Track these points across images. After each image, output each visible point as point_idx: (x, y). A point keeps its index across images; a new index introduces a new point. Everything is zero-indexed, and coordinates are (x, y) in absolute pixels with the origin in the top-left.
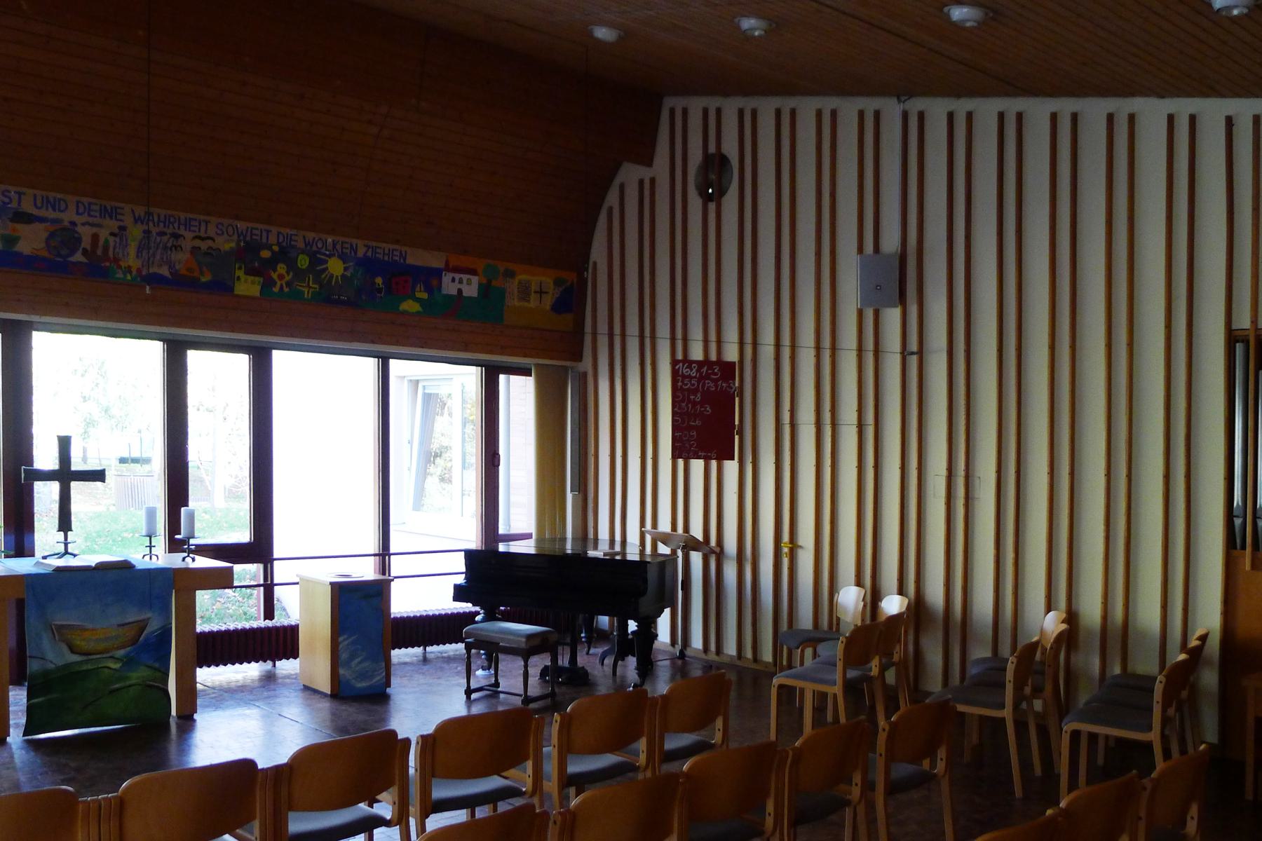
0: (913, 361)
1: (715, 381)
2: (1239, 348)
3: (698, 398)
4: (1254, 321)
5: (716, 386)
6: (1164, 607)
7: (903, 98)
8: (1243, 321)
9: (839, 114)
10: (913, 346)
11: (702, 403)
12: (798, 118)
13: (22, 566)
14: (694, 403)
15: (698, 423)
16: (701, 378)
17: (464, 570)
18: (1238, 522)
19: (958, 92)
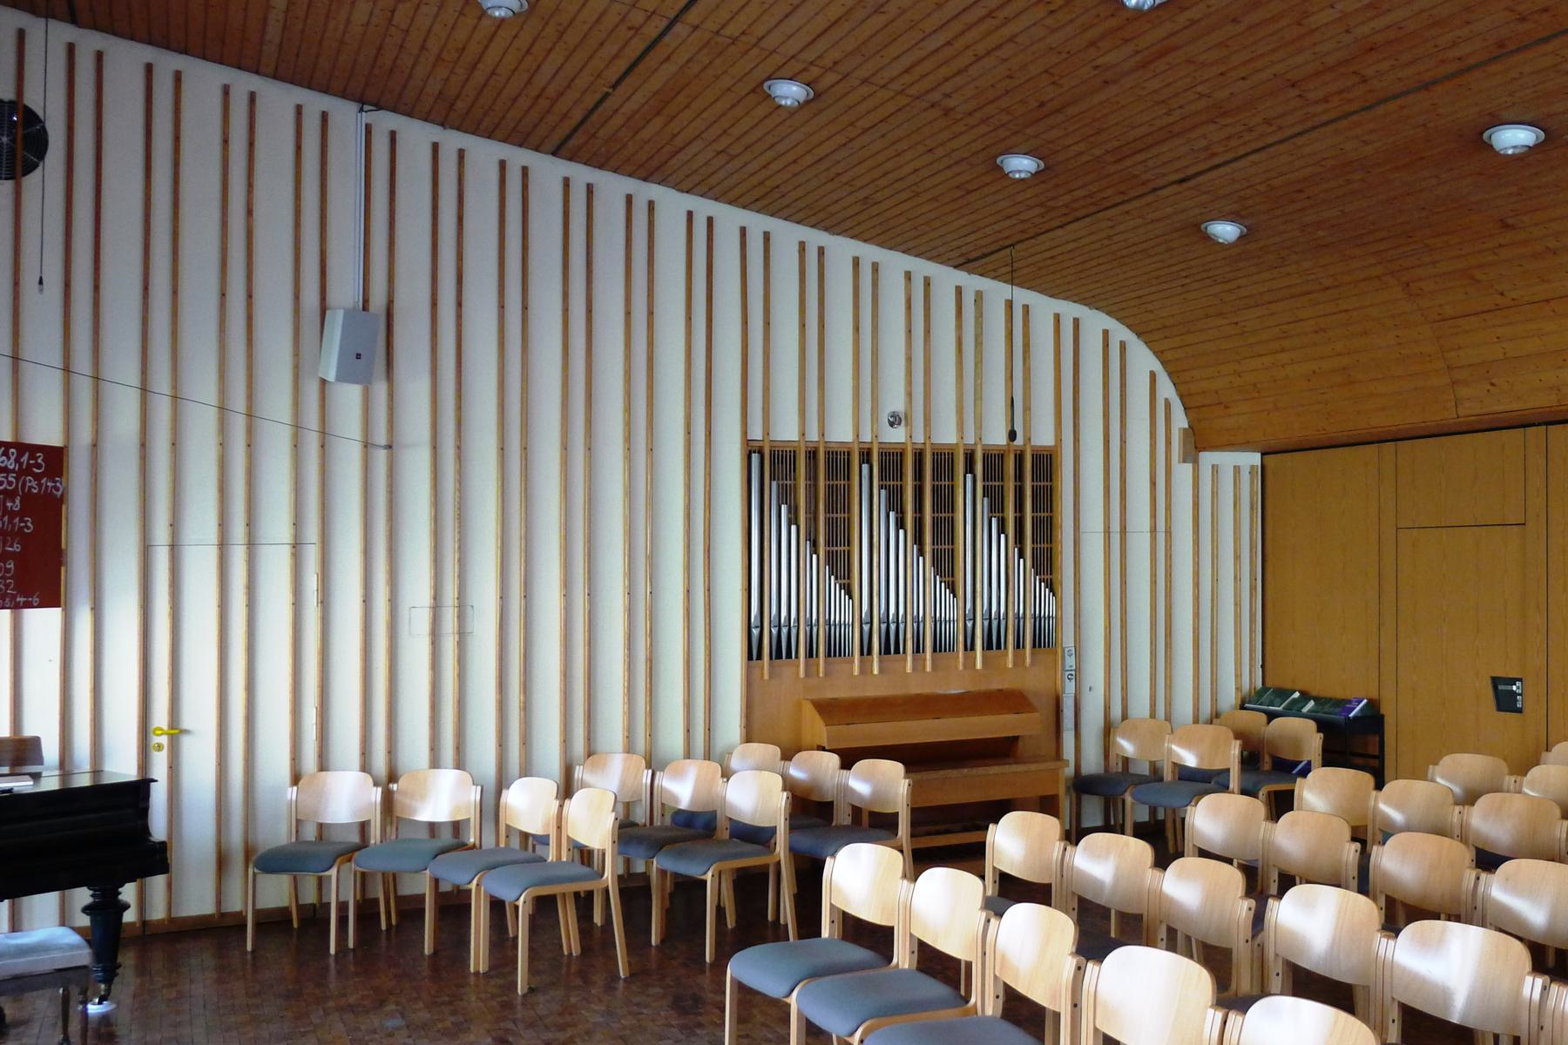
0: (381, 457)
1: (37, 477)
2: (755, 457)
3: (16, 505)
4: (767, 432)
5: (40, 485)
6: (688, 731)
7: (366, 107)
8: (756, 433)
9: (305, 110)
10: (381, 437)
11: (22, 514)
12: (184, 86)
13: (23, 785)
14: (12, 514)
15: (17, 548)
16: (22, 472)
17: (107, 780)
18: (755, 632)
19: (521, 139)
